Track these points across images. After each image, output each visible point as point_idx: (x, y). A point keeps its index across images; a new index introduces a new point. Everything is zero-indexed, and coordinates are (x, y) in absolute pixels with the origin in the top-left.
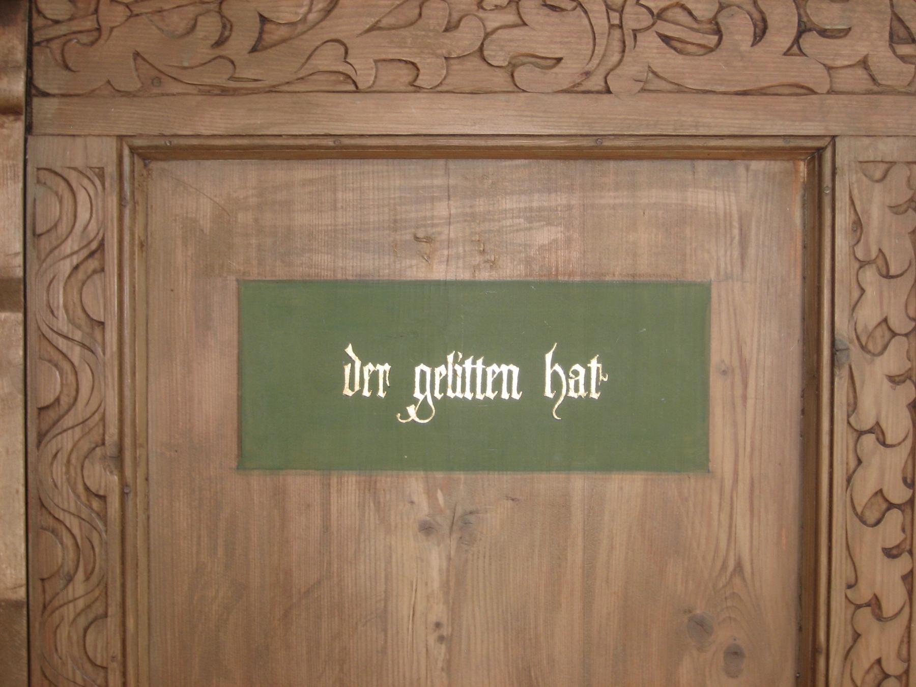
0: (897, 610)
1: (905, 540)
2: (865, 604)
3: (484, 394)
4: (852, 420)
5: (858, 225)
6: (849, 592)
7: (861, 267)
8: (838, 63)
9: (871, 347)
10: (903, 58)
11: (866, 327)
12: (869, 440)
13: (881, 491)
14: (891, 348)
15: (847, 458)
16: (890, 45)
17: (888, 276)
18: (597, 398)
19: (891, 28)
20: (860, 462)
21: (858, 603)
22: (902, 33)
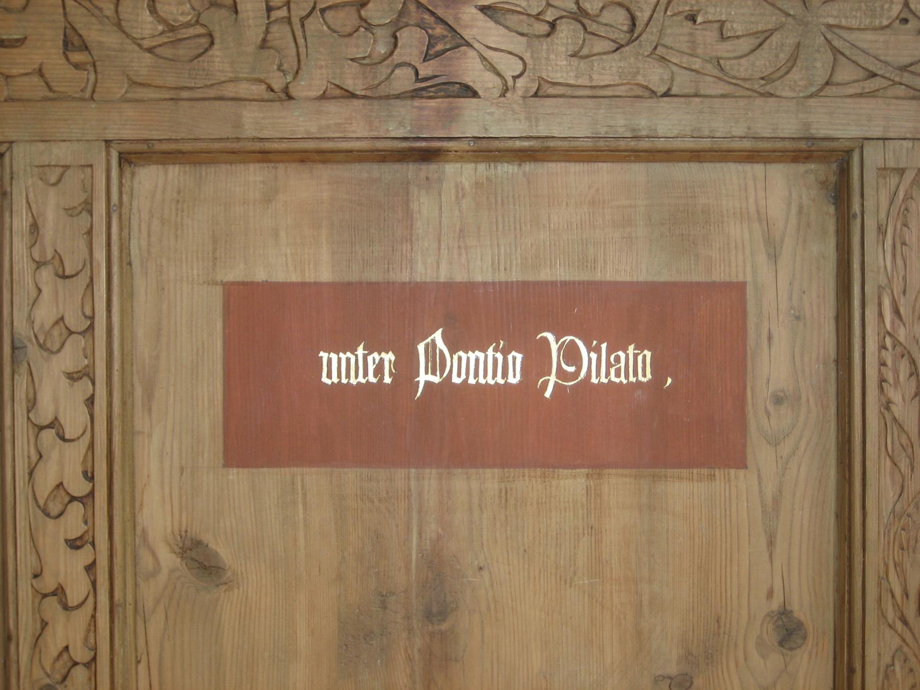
0: (81, 599)
1: (86, 532)
2: (52, 593)
3: (367, 378)
4: (31, 415)
5: (35, 228)
6: (34, 582)
7: (38, 268)
8: (14, 72)
9: (49, 345)
10: (77, 66)
11: (42, 325)
12: (48, 436)
13: (61, 484)
14: (67, 345)
15: (29, 452)
16: (64, 53)
17: (64, 277)
18: (385, 381)
19: (65, 36)
20: (41, 456)
21: (44, 592)
22: (76, 41)
